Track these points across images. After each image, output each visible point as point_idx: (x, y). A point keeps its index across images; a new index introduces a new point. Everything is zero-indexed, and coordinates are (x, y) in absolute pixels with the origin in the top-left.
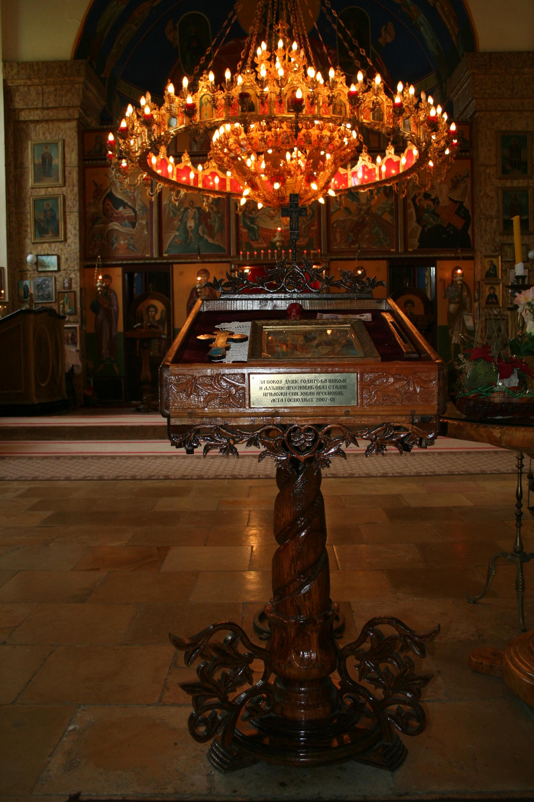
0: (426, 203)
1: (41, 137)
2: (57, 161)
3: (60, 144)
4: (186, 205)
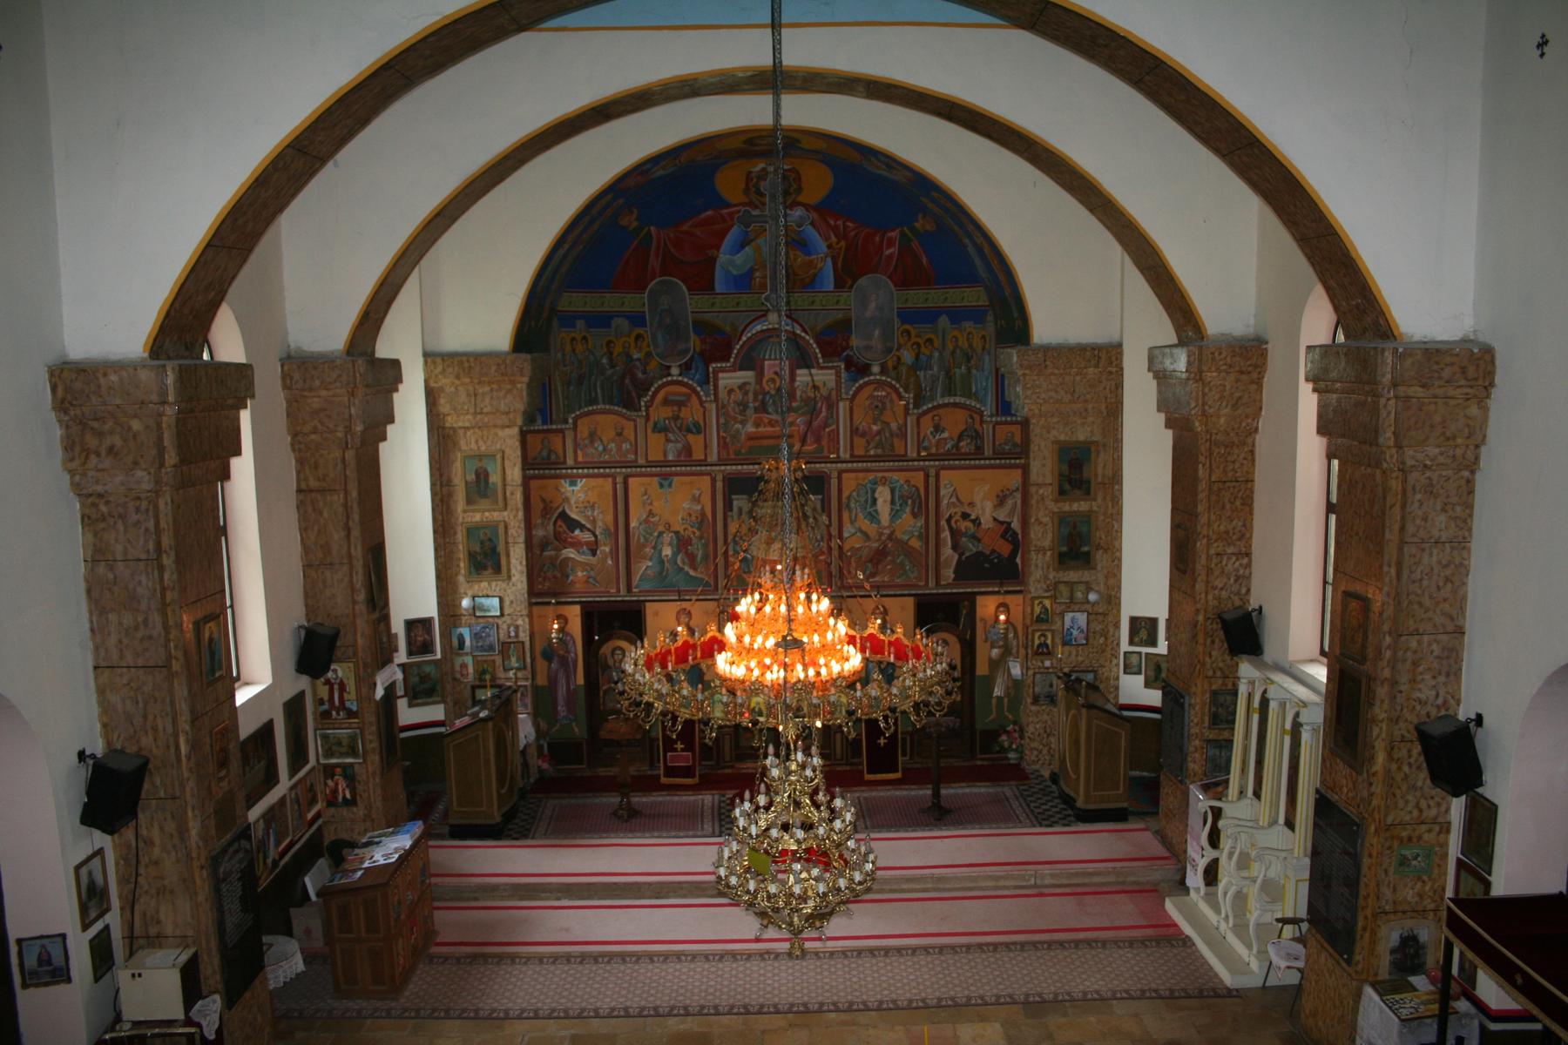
0: (964, 525)
1: (474, 446)
2: (495, 478)
3: (499, 456)
4: (661, 528)
